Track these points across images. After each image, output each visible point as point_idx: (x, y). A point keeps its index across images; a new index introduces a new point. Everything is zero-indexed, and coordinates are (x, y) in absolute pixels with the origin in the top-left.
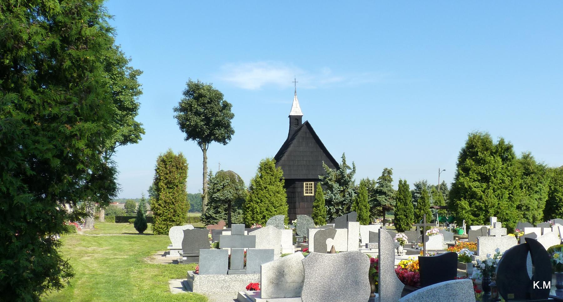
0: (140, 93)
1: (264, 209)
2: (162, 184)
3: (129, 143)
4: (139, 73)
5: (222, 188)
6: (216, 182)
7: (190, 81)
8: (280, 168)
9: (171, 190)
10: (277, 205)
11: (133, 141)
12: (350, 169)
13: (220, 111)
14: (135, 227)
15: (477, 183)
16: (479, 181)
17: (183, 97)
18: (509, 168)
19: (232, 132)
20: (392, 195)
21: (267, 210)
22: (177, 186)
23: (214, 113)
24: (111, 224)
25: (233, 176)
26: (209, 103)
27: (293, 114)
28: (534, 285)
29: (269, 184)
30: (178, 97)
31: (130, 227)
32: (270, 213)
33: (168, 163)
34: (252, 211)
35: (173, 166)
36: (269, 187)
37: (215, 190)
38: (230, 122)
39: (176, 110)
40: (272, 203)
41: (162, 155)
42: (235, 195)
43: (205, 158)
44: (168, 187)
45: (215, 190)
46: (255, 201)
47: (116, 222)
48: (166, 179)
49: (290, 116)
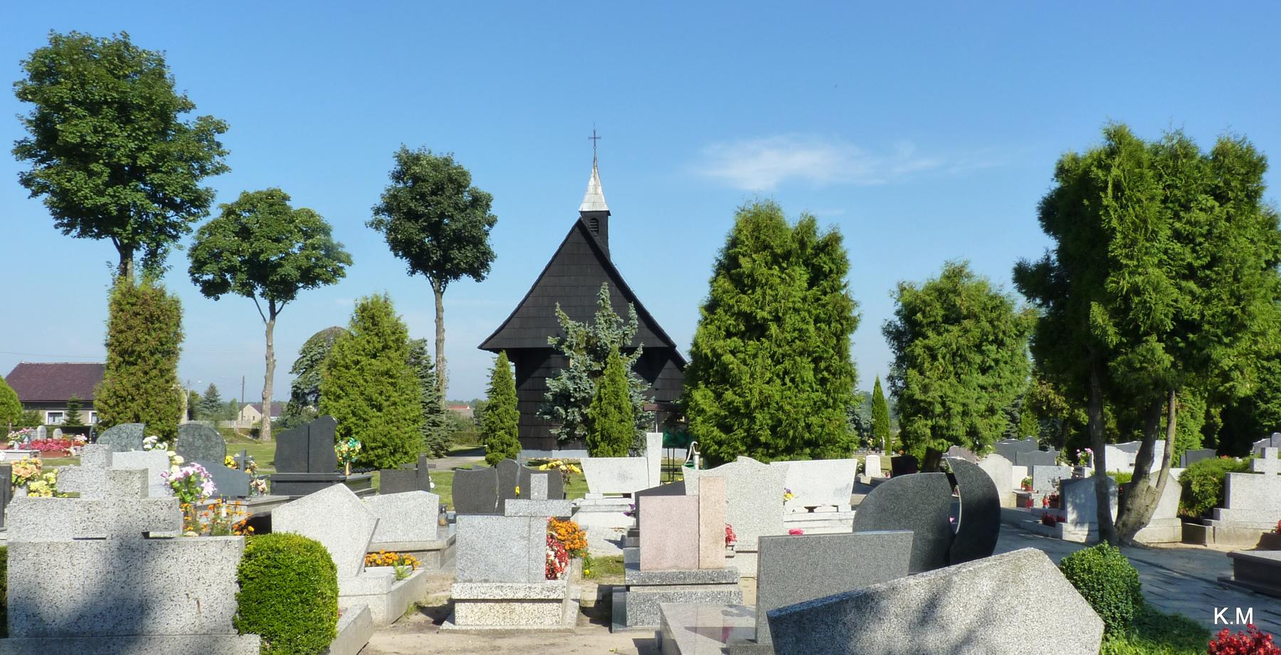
15: (736, 342)
16: (742, 335)
18: (826, 299)
28: (1216, 616)
32: (361, 422)
43: (439, 310)
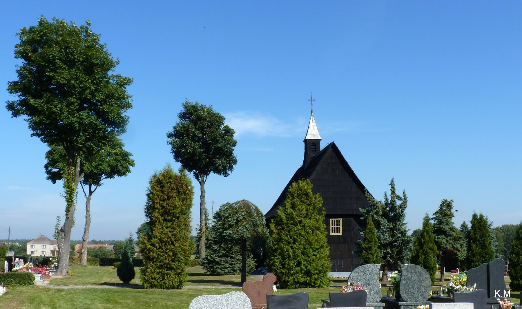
0: (129, 106)
1: (299, 252)
2: (157, 215)
3: (116, 176)
4: (129, 81)
5: (236, 223)
6: (227, 215)
7: (187, 103)
8: (318, 195)
9: (169, 224)
10: (317, 247)
11: (121, 173)
12: (401, 200)
13: (222, 137)
14: (119, 275)
17: (179, 120)
19: (235, 162)
20: (455, 235)
21: (303, 253)
22: (178, 218)
23: (215, 138)
24: (95, 267)
25: (250, 207)
26: (209, 127)
27: (309, 137)
29: (305, 217)
30: (172, 121)
31: (111, 274)
32: (306, 258)
33: (166, 185)
34: (282, 254)
35: (172, 189)
36: (307, 221)
37: (226, 226)
38: (233, 150)
39: (170, 136)
40: (310, 244)
41: (158, 174)
42: (253, 233)
44: (165, 220)
45: (226, 226)
46: (285, 240)
47: (101, 265)
48: (163, 207)
49: (306, 141)
